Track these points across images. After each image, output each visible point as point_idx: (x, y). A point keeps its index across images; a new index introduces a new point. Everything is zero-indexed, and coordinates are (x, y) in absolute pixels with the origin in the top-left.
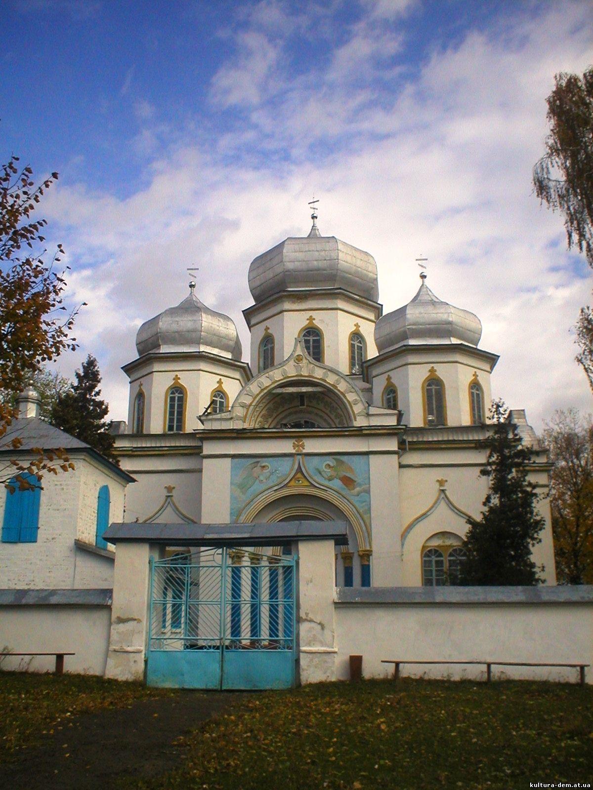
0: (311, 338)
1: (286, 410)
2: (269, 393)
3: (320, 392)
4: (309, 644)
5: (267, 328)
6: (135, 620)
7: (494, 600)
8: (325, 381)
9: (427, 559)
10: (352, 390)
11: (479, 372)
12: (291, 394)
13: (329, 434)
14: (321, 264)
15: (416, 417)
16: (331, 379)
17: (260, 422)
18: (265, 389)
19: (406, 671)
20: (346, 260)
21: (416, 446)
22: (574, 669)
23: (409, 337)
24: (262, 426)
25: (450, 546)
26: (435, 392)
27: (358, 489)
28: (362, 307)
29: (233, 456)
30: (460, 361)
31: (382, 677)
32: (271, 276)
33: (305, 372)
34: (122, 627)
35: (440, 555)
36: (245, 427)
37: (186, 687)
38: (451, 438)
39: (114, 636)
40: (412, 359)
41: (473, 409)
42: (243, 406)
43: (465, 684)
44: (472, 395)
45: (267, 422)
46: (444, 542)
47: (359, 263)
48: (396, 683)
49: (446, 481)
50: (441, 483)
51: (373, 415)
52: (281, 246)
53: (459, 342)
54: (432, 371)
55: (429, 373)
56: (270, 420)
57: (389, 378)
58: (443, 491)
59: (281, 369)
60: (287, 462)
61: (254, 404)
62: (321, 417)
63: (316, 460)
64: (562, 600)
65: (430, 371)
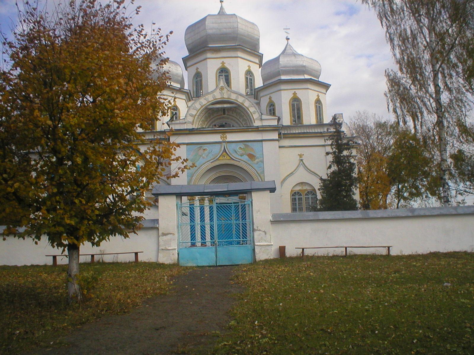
0: (295, 103)
1: (215, 117)
2: (206, 108)
3: (234, 107)
4: (259, 242)
5: (197, 69)
6: (171, 234)
7: (348, 217)
8: (237, 101)
9: (293, 197)
10: (252, 106)
11: (320, 94)
12: (218, 108)
13: (241, 130)
14: (228, 31)
15: (286, 120)
16: (233, 97)
17: (201, 124)
18: (203, 106)
19: (307, 252)
20: (242, 28)
21: (287, 136)
22: (385, 248)
23: (281, 74)
24: (202, 127)
25: (306, 190)
26: (296, 107)
27: (257, 160)
28: (252, 56)
29: (187, 144)
30: (310, 88)
31: (295, 255)
32: (199, 37)
33: (226, 96)
34: (165, 238)
35: (301, 195)
36: (193, 127)
37: (199, 265)
38: (305, 131)
39: (161, 243)
40: (283, 87)
41: (317, 115)
42: (191, 115)
43: (334, 257)
44: (316, 107)
45: (205, 124)
46: (302, 188)
47: (250, 30)
48: (302, 258)
49: (303, 155)
50: (301, 156)
51: (264, 120)
52: (204, 19)
53: (309, 77)
54: (295, 94)
55: (293, 95)
56: (206, 123)
57: (270, 98)
58: (302, 160)
59: (212, 95)
60: (218, 146)
61: (198, 114)
62: (234, 121)
63: (233, 145)
64: (379, 217)
65: (293, 94)
